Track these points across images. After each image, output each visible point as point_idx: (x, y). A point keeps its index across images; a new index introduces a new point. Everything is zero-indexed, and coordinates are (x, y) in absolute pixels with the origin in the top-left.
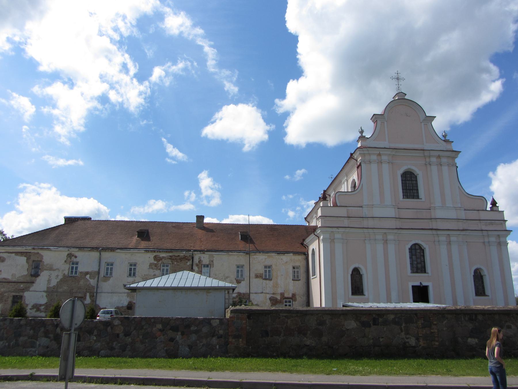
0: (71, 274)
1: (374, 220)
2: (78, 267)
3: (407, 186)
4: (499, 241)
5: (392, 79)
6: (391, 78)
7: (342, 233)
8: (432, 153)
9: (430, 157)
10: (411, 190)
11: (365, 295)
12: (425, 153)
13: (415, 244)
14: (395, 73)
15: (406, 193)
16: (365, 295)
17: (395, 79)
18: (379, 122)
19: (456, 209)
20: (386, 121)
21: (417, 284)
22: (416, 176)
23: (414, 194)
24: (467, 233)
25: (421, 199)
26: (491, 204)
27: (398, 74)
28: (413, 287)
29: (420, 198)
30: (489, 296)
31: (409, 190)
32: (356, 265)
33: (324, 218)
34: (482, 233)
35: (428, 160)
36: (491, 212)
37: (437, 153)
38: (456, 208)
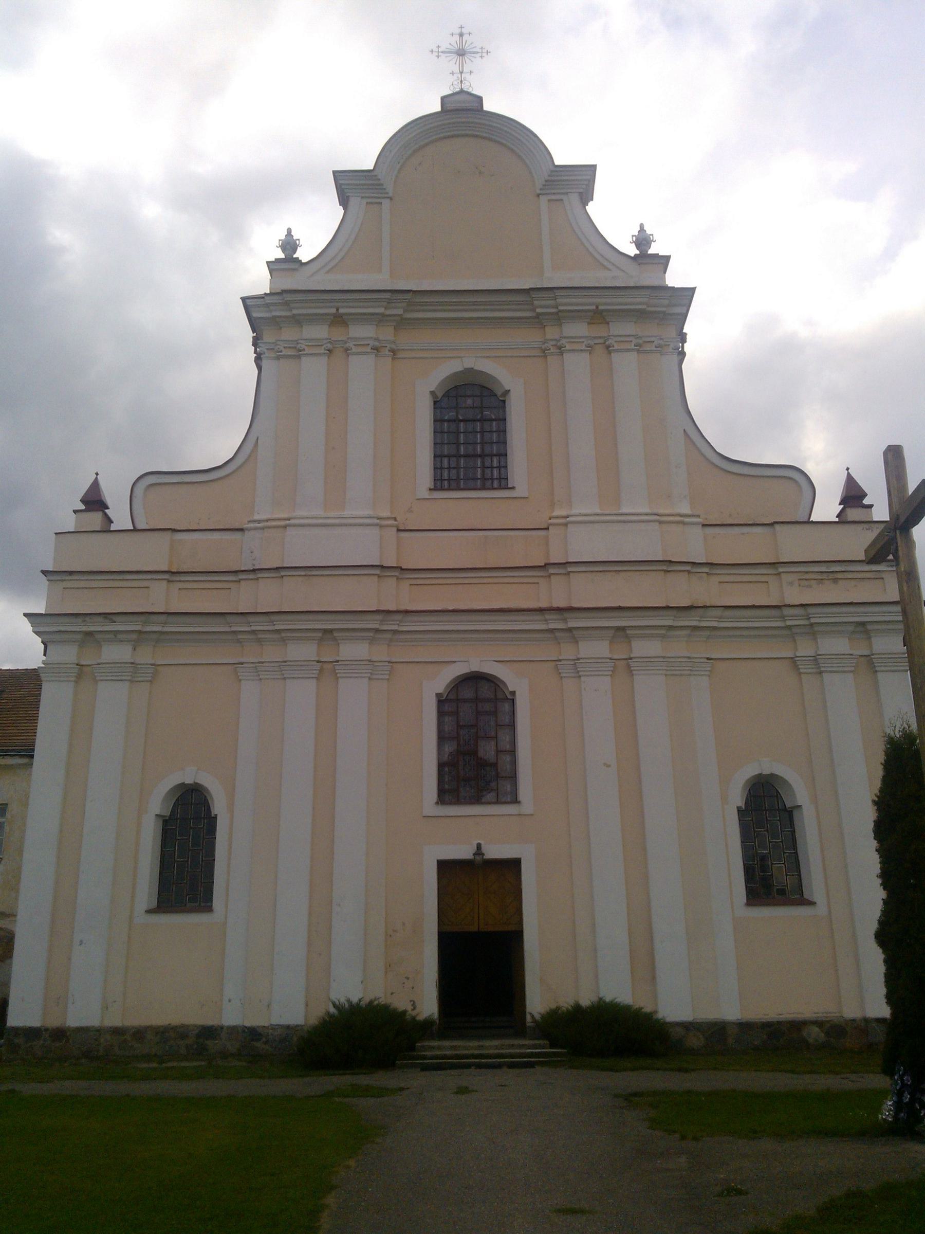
1: (779, 574)
3: (484, 467)
5: (484, 54)
6: (432, 51)
7: (134, 636)
11: (811, 903)
13: (475, 679)
16: (811, 903)
17: (471, 53)
21: (464, 852)
23: (488, 471)
26: (82, 501)
27: (461, 35)
28: (445, 867)
29: (510, 486)
31: (464, 456)
32: (767, 767)
33: (62, 581)
34: (783, 618)
36: (840, 527)
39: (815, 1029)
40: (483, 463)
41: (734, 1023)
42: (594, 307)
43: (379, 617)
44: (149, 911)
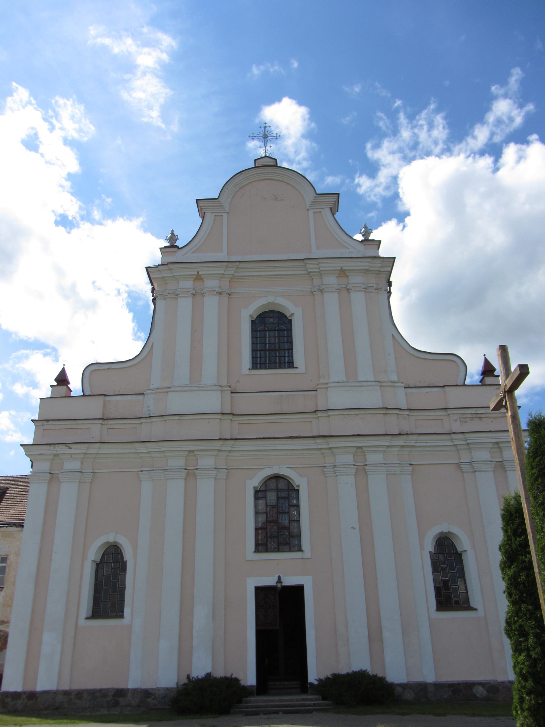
0: (112, 580)
2: (5, 567)
3: (265, 344)
4: (500, 460)
7: (82, 456)
8: (325, 265)
9: (321, 274)
10: (275, 350)
12: (307, 266)
13: (277, 478)
14: (261, 127)
15: (263, 359)
18: (208, 216)
19: (381, 386)
20: (228, 213)
21: (270, 581)
22: (291, 320)
23: (282, 358)
24: (411, 441)
25: (297, 368)
28: (258, 590)
29: (294, 367)
30: (476, 609)
32: (111, 538)
33: (43, 425)
35: (317, 282)
37: (337, 265)
38: (380, 383)
39: (480, 688)
40: (279, 354)
41: (432, 684)
42: (340, 268)
43: (221, 442)
44: (87, 618)
